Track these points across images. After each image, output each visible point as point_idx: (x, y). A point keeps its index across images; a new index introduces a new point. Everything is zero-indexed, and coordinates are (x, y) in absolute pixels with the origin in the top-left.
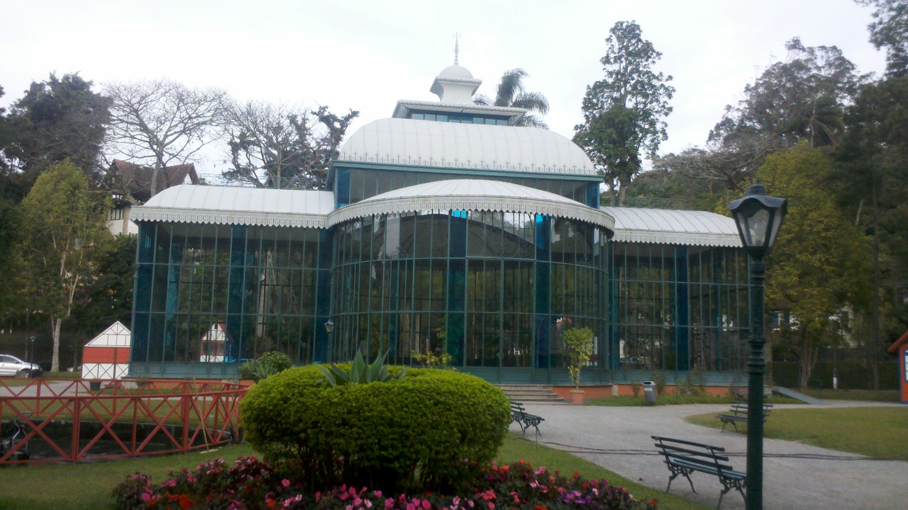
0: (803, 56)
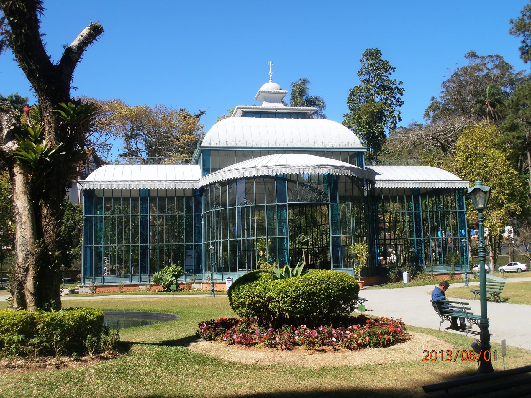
0: (478, 61)
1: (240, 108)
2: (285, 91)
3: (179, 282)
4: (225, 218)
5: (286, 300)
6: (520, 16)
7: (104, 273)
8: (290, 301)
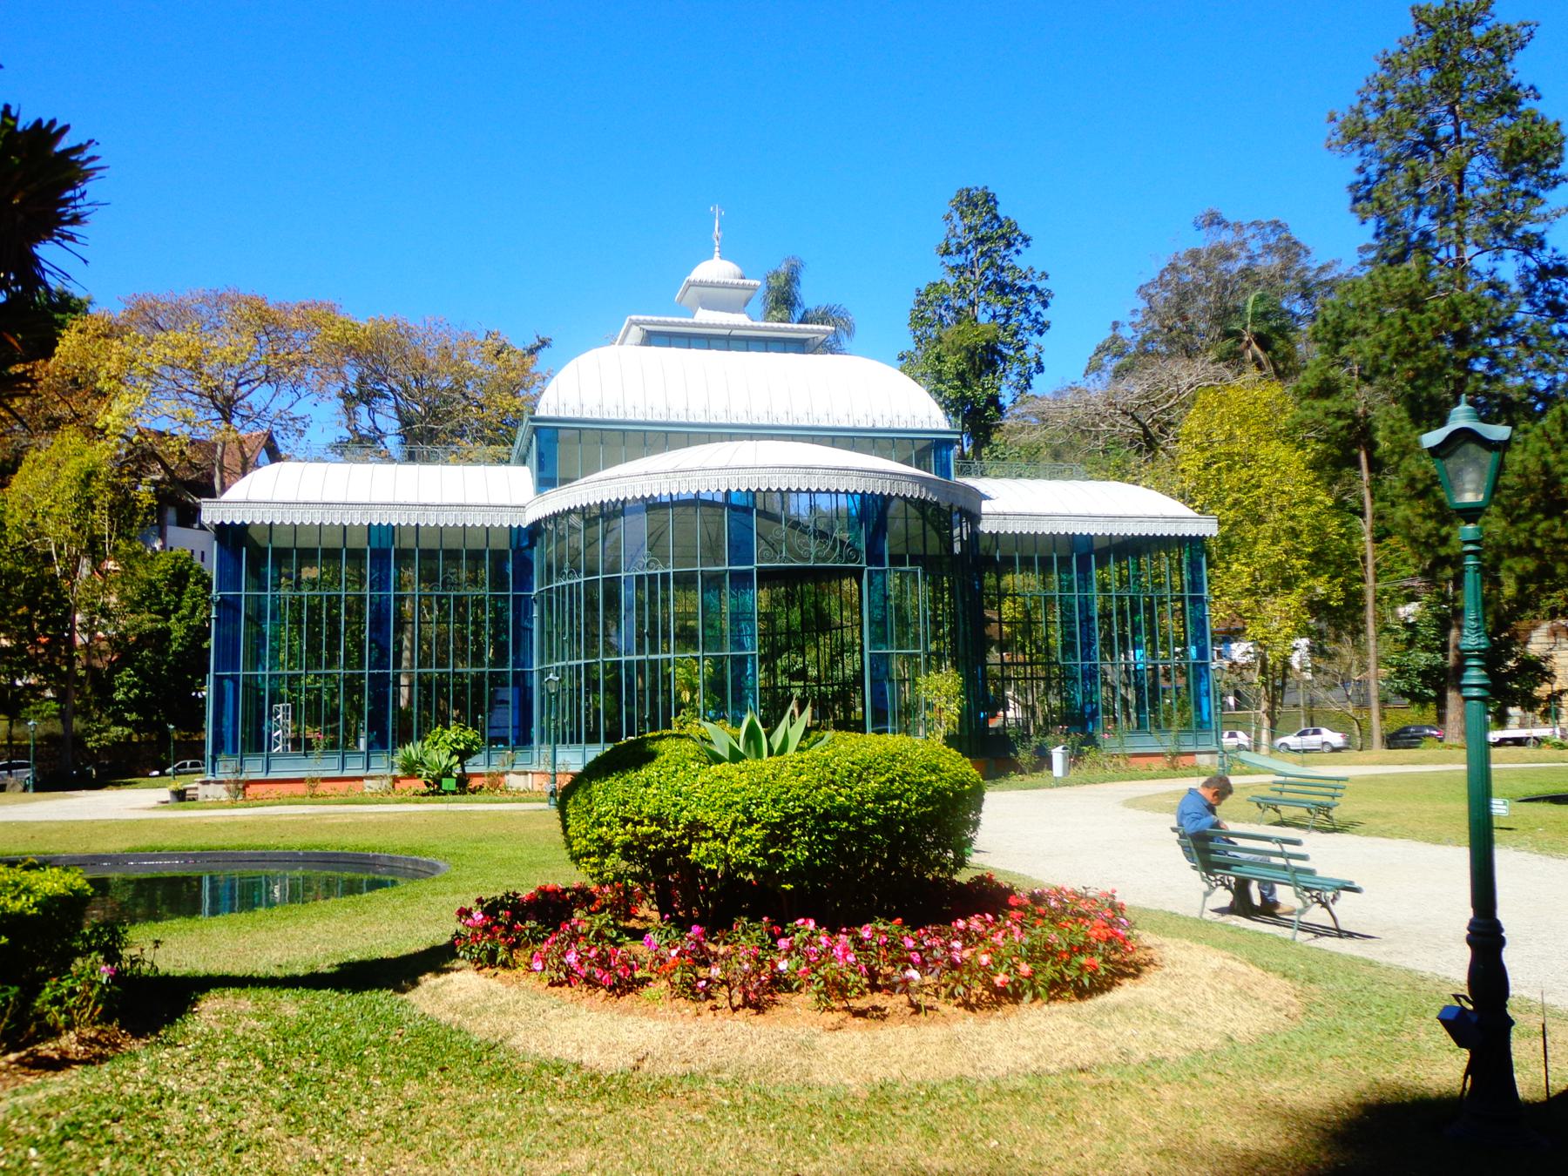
0: (1227, 236)
1: (637, 323)
2: (753, 282)
3: (468, 770)
4: (591, 605)
5: (748, 832)
6: (1356, 103)
7: (276, 745)
8: (761, 834)
